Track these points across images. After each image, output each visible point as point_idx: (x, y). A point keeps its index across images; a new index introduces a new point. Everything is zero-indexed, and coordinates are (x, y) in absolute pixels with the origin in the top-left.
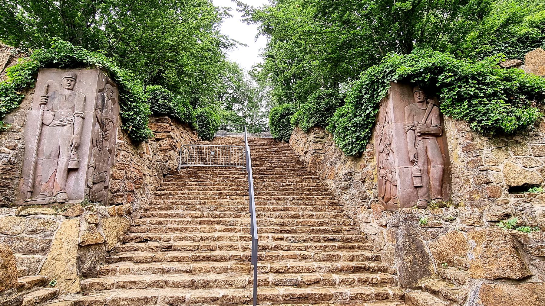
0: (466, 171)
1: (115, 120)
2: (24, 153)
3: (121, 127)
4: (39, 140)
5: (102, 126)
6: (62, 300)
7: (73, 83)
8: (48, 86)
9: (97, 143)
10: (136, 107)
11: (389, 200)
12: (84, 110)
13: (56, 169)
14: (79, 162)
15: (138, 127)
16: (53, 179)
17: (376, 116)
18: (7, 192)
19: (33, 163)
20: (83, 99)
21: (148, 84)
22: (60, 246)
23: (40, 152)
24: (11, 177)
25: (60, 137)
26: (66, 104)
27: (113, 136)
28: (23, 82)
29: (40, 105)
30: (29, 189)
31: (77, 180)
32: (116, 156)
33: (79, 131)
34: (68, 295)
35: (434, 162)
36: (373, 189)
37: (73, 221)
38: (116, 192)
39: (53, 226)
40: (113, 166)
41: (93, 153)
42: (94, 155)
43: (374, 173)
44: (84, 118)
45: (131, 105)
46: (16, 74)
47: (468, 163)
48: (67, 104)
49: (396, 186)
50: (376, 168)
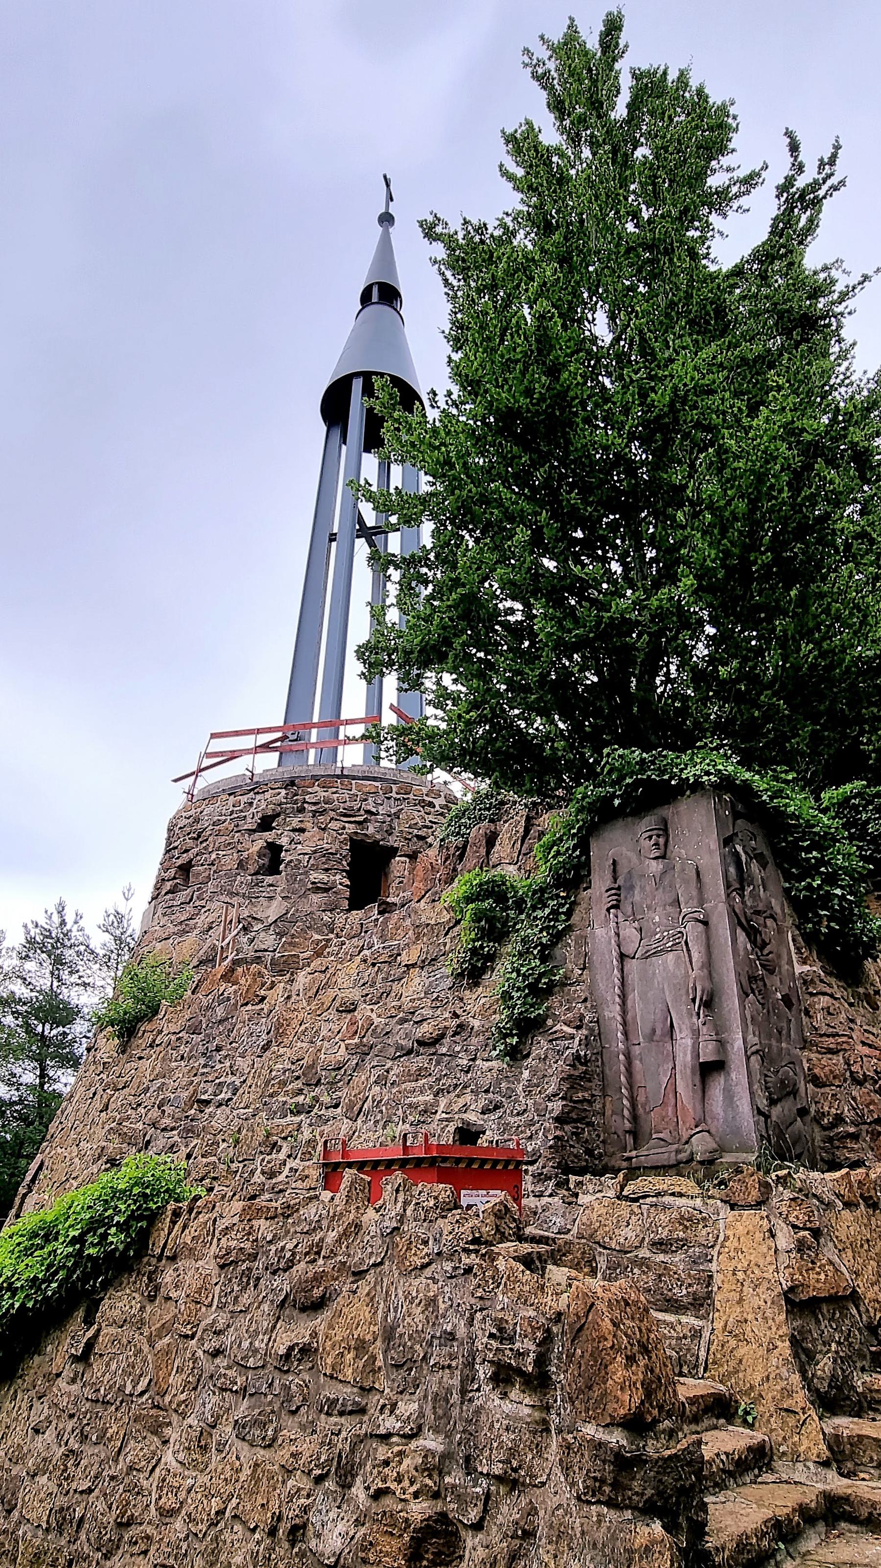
1: (777, 909)
2: (599, 1034)
3: (798, 928)
4: (623, 997)
5: (752, 933)
6: (785, 1477)
7: (661, 841)
8: (614, 863)
9: (752, 984)
10: (821, 862)
12: (701, 902)
13: (674, 1068)
14: (722, 1044)
15: (845, 917)
16: (671, 1096)
19: (621, 1057)
21: (822, 789)
22: (737, 1296)
23: (630, 1028)
25: (665, 979)
26: (659, 894)
27: (785, 957)
28: (568, 866)
29: (608, 910)
30: (628, 1125)
31: (729, 1096)
32: (807, 1013)
33: (705, 959)
34: (800, 1466)
37: (750, 1219)
39: (704, 1232)
40: (806, 1044)
41: (748, 1013)
44: (705, 923)
45: (808, 860)
46: (552, 853)
48: (661, 896)
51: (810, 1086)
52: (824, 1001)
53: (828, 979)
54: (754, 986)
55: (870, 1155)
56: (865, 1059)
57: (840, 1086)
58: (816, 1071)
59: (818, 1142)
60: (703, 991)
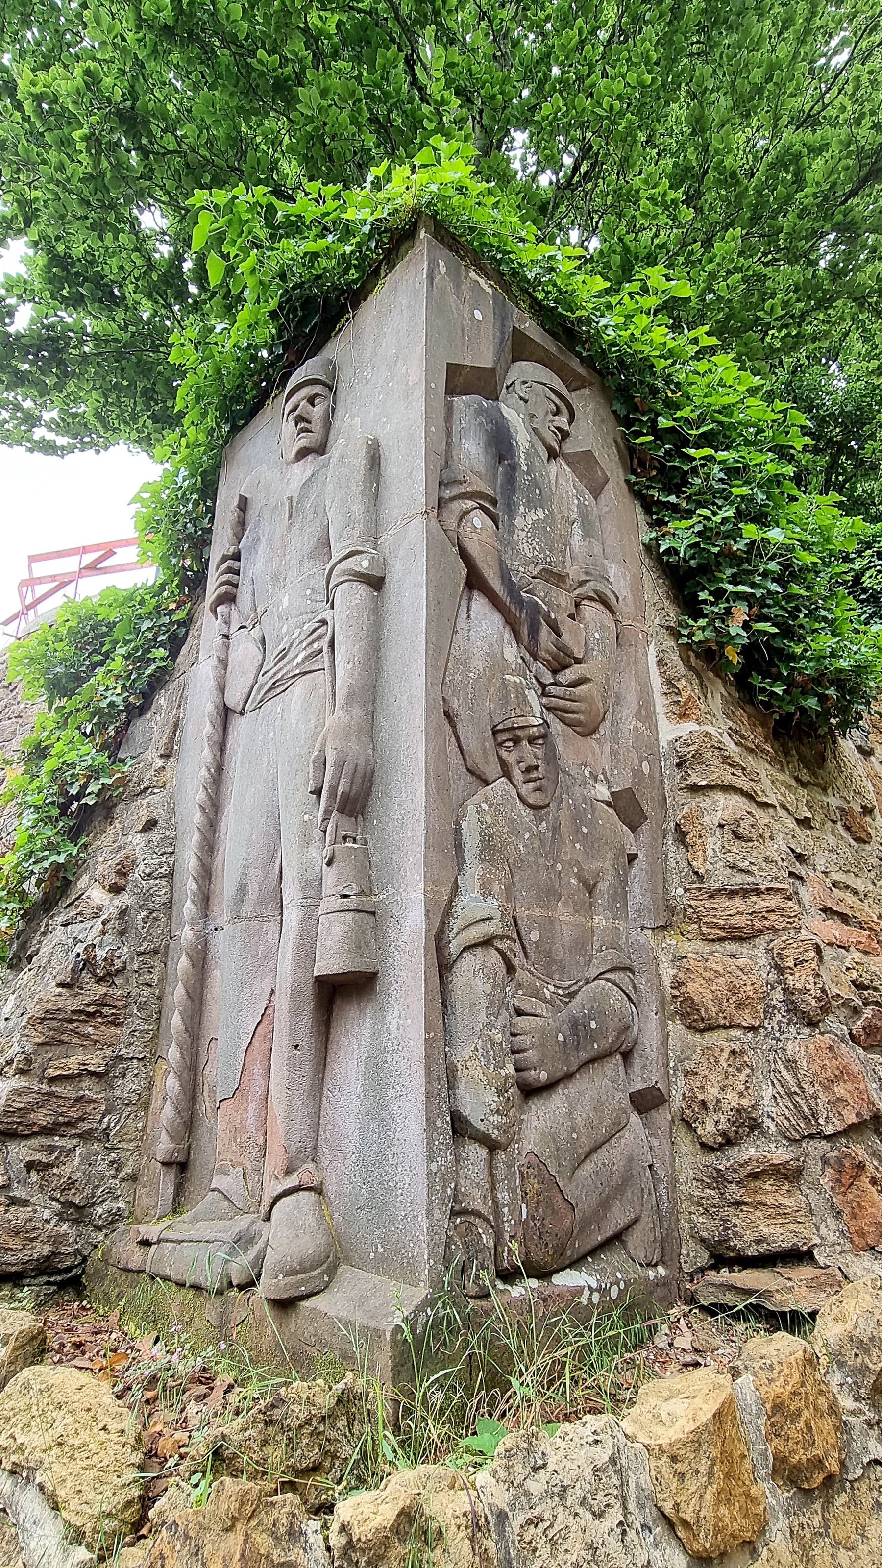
3: (675, 634)
5: (523, 620)
14: (370, 915)
16: (258, 1070)
18: (71, 1168)
20: (360, 461)
24: (95, 1061)
32: (681, 836)
38: (729, 1142)
42: (489, 847)
51: (676, 1028)
52: (726, 806)
53: (751, 762)
54: (511, 758)
55: (830, 1230)
56: (828, 952)
57: (753, 1029)
58: (693, 988)
59: (688, 1187)
60: (340, 766)
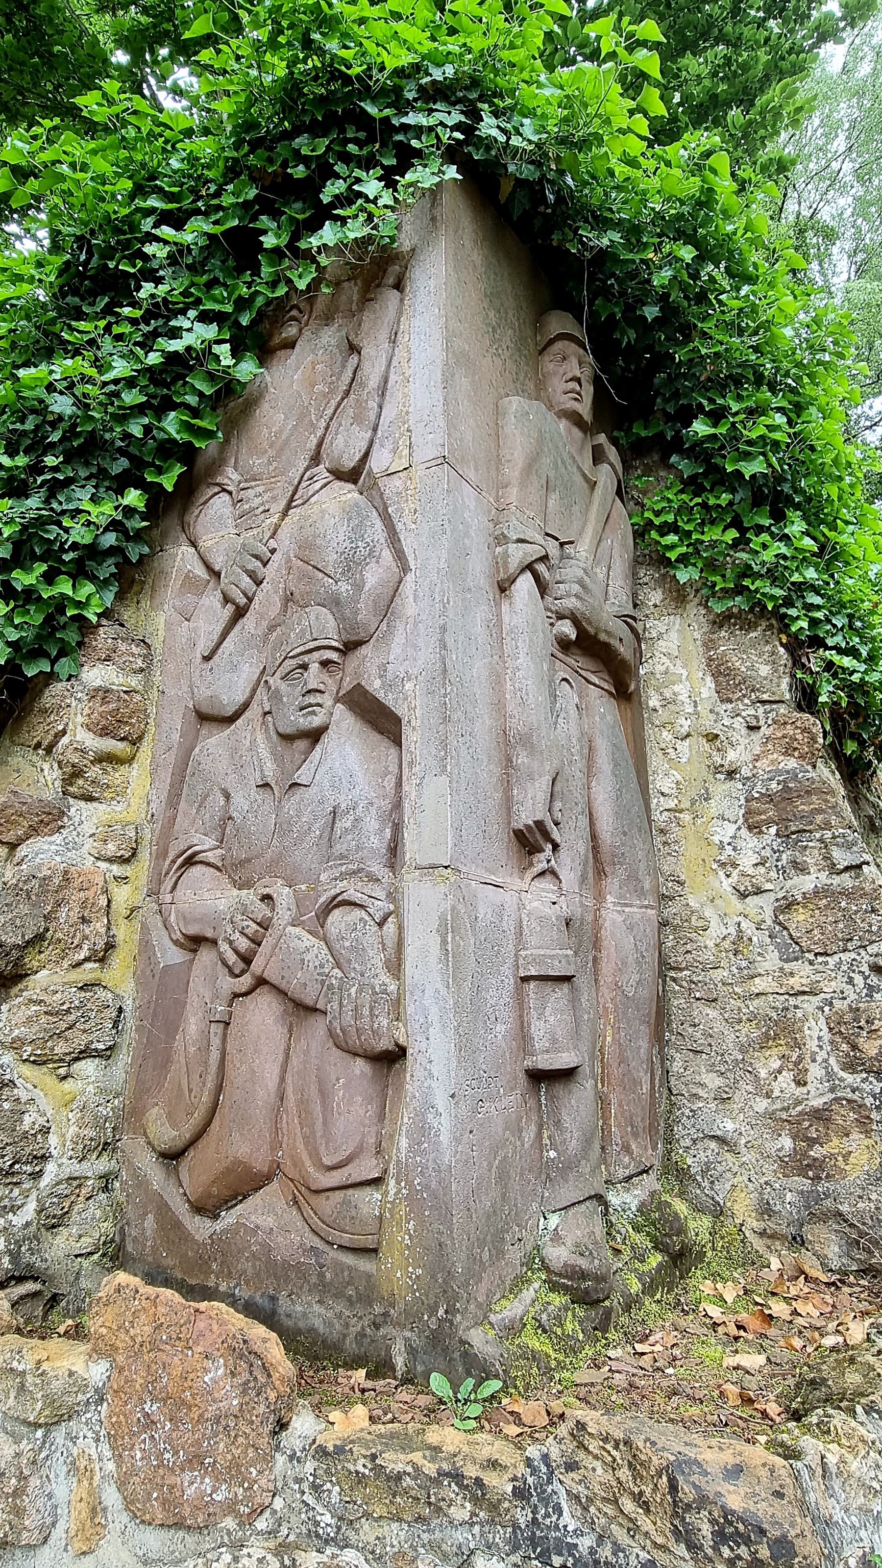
0: (772, 960)
11: (242, 1185)
17: (231, 402)
35: (621, 871)
36: (85, 1053)
43: (122, 896)
47: (787, 905)
49: (391, 1059)
50: (145, 855)
